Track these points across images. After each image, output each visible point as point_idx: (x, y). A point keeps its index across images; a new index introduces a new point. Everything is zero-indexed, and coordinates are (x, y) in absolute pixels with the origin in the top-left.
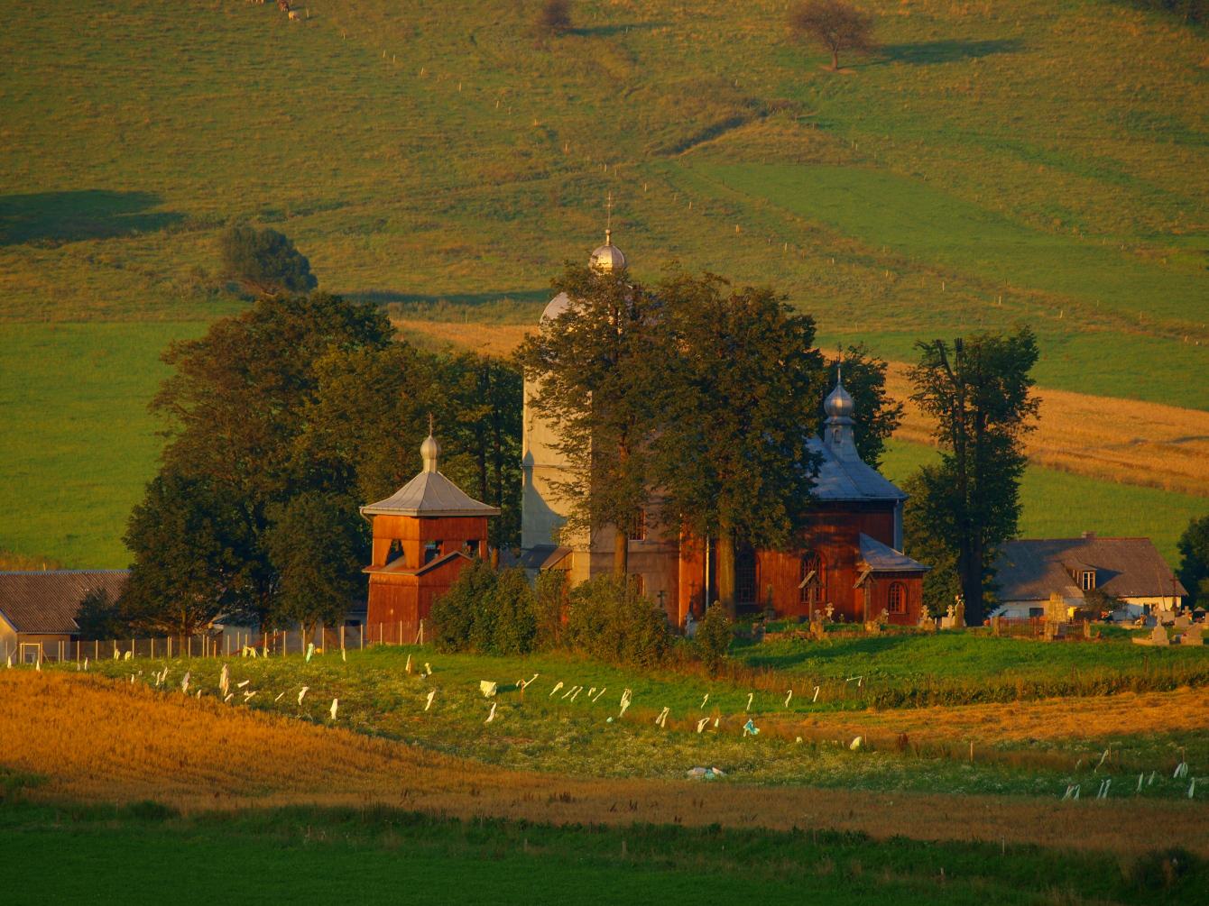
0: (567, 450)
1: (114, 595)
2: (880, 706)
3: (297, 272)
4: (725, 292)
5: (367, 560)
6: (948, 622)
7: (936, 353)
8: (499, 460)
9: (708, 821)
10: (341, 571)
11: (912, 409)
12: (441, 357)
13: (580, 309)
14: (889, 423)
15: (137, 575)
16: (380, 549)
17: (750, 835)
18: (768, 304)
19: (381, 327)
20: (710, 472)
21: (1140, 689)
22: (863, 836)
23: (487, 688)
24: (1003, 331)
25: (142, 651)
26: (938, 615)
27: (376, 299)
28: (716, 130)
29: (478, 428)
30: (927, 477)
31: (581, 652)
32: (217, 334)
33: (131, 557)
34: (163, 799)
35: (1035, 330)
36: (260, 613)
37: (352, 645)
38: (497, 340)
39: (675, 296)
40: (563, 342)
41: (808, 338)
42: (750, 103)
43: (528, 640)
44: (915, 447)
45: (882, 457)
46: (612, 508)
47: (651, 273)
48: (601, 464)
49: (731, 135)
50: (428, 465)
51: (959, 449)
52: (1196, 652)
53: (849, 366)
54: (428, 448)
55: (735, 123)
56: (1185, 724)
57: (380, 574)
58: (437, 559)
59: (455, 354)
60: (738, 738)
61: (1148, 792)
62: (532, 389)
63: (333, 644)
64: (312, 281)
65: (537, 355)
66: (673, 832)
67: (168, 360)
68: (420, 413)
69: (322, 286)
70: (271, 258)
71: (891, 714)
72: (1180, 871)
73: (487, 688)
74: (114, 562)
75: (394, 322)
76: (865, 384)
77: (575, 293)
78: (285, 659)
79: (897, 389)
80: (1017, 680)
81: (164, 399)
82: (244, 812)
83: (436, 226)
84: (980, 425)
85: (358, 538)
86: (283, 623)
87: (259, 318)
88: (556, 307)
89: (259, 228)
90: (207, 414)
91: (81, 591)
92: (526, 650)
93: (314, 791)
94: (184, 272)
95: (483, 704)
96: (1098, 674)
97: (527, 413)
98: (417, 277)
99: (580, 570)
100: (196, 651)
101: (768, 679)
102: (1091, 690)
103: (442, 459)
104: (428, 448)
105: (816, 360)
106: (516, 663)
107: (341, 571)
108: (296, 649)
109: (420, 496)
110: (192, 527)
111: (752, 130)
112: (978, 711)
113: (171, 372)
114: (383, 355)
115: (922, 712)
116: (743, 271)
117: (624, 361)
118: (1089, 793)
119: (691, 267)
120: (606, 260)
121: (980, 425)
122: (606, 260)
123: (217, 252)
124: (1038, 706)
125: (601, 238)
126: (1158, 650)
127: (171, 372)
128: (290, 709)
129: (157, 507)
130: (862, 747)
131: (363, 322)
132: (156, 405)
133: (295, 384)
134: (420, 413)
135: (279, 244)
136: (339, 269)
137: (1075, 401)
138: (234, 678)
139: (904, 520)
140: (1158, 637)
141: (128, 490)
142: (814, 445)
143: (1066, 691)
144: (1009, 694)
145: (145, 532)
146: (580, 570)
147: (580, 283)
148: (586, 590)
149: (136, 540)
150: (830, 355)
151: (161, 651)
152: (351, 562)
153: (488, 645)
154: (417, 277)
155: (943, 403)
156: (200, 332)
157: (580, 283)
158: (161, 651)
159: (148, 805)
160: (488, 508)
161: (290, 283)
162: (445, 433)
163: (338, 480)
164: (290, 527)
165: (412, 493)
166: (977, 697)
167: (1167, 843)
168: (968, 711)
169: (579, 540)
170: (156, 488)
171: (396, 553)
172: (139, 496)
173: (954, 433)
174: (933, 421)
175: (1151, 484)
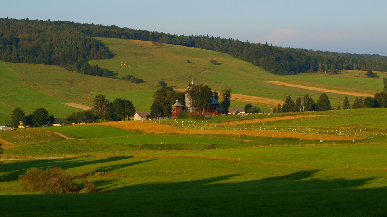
0: (189, 100)
1: (149, 114)
2: (218, 122)
3: (166, 85)
4: (203, 86)
5: (172, 111)
6: (224, 115)
7: (222, 91)
8: (183, 101)
9: (202, 133)
10: (170, 112)
11: (220, 96)
12: (178, 92)
13: (190, 88)
14: (218, 97)
15: (151, 112)
16: (173, 109)
17: (206, 134)
18: (207, 87)
19: (172, 90)
20: (202, 102)
21: (241, 120)
22: (216, 134)
23: (183, 122)
24: (228, 89)
25: (152, 119)
26: (223, 114)
27: (172, 87)
28: (203, 71)
29: (181, 98)
30: (222, 102)
31: (191, 118)
32: (158, 91)
33: (151, 111)
34: (154, 132)
35: (231, 88)
36: (163, 116)
37: (171, 118)
38: (183, 90)
39: (199, 86)
40: (189, 91)
41: (211, 90)
42: (206, 69)
43: (186, 117)
44: (221, 99)
45: (218, 100)
46: (193, 105)
47: (196, 84)
48: (193, 101)
49: (204, 71)
50: (177, 102)
51: (225, 100)
52: (246, 117)
53: (214, 92)
54: (177, 100)
55: (205, 70)
56: (245, 123)
57: (173, 112)
58: (178, 110)
59: (180, 92)
60: (205, 126)
61: (242, 129)
62: (186, 95)
63: (169, 118)
64: (167, 86)
65: (186, 92)
66: (199, 134)
67: (154, 93)
68: (176, 97)
69: (168, 86)
70: (163, 84)
71: (219, 123)
72: (244, 136)
73: (183, 122)
74: (149, 112)
75: (174, 89)
76: (216, 94)
77: (190, 86)
78: (165, 120)
79: (219, 94)
80: (230, 120)
81: (153, 97)
82: (161, 133)
83: (178, 80)
84: (226, 97)
85: (171, 108)
86: (164, 116)
87: (162, 89)
88: (188, 87)
89: (162, 81)
90: (157, 98)
91: (146, 114)
92: (186, 118)
93: (167, 131)
94: (155, 85)
95: (182, 123)
96: (237, 119)
97: (186, 97)
98: (176, 85)
99: (191, 111)
100: (157, 119)
101: (208, 120)
102: (236, 121)
103: (178, 101)
104: (177, 100)
105: (211, 92)
106: (185, 119)
107: (170, 112)
108: (166, 119)
109: (176, 105)
110: (156, 108)
111: (206, 71)
112: (227, 123)
113: (154, 94)
114: (173, 92)
115: (221, 123)
116: (205, 84)
117: (194, 92)
118: (236, 130)
119: (200, 83)
120: (192, 83)
121: (226, 97)
122: (192, 83)
123: (158, 83)
124: (232, 122)
125: (176, 98)
126: (242, 117)
127: (154, 94)
128: (165, 124)
129: (153, 106)
130: (216, 126)
131: (171, 89)
132: (289, 95)
133: (165, 95)
134: (176, 97)
135: (164, 82)
136: (169, 85)
137: (235, 94)
138: (160, 121)
139: (220, 106)
140: (243, 116)
141: (150, 105)
142: (211, 99)
143: (234, 121)
144: (229, 121)
145: (152, 108)
146: (191, 111)
147: (190, 85)
148: (191, 113)
149: (151, 109)
150: (213, 91)
151: (154, 119)
152: (170, 111)
153: (183, 118)
154: (176, 85)
155: (223, 95)
156: (156, 90)
157: (190, 85)
158: (154, 119)
159: (153, 133)
160: (182, 106)
161: (165, 86)
162: (178, 99)
163: (169, 103)
164: (165, 108)
165: (176, 105)
166: (226, 121)
167: (242, 134)
168: (225, 123)
169: (191, 108)
170: (153, 105)
171: (174, 110)
172: (152, 105)
173: (224, 97)
174: (222, 97)
175: (242, 102)
